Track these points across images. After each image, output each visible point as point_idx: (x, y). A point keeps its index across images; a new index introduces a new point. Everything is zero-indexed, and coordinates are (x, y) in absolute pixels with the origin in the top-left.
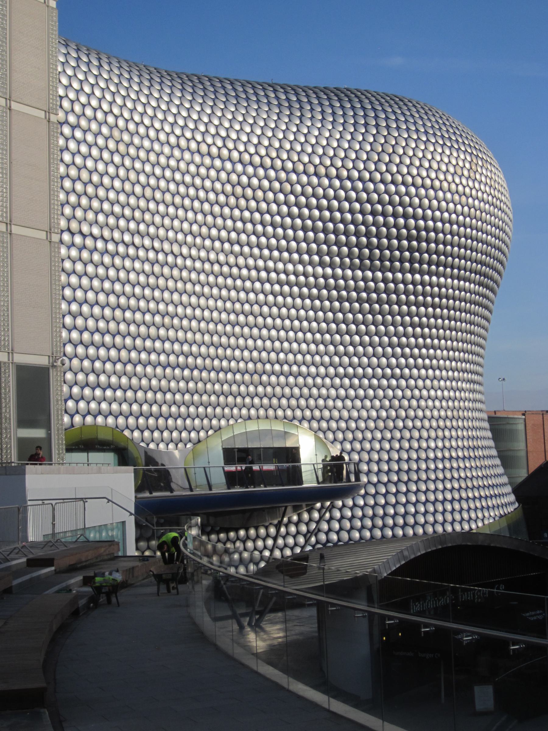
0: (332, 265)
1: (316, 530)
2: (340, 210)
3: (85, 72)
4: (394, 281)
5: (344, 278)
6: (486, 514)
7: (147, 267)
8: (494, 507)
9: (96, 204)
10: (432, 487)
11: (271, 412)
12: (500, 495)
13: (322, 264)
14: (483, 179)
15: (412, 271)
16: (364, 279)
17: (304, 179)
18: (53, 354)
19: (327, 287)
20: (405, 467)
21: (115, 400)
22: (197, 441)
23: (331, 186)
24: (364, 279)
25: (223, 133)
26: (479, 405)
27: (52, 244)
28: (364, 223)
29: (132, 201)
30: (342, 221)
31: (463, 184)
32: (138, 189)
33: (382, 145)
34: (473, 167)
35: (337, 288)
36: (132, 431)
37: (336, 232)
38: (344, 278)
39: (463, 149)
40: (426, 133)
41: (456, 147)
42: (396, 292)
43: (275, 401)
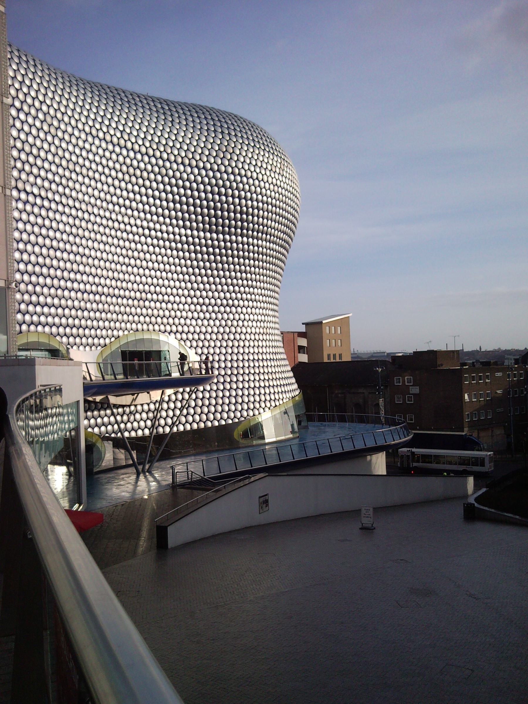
0: (191, 228)
1: (187, 406)
2: (198, 190)
3: (26, 69)
4: (231, 241)
5: (198, 237)
6: (285, 396)
7: (71, 221)
8: (285, 392)
9: (35, 171)
10: (252, 378)
11: (151, 327)
12: (289, 384)
13: (184, 227)
14: (288, 176)
15: (242, 235)
16: (212, 239)
17: (175, 166)
18: (8, 278)
19: (187, 243)
20: (235, 365)
21: (50, 315)
22: (104, 345)
23: (192, 173)
24: (212, 239)
25: (121, 128)
26: (277, 326)
27: (7, 197)
28: (213, 200)
29: (60, 171)
30: (199, 198)
31: (275, 178)
32: (64, 163)
33: (226, 146)
34: (282, 167)
35: (194, 244)
36: (62, 337)
37: (194, 205)
38: (198, 237)
39: (276, 154)
40: (253, 140)
41: (272, 152)
42: (231, 249)
43: (153, 319)
